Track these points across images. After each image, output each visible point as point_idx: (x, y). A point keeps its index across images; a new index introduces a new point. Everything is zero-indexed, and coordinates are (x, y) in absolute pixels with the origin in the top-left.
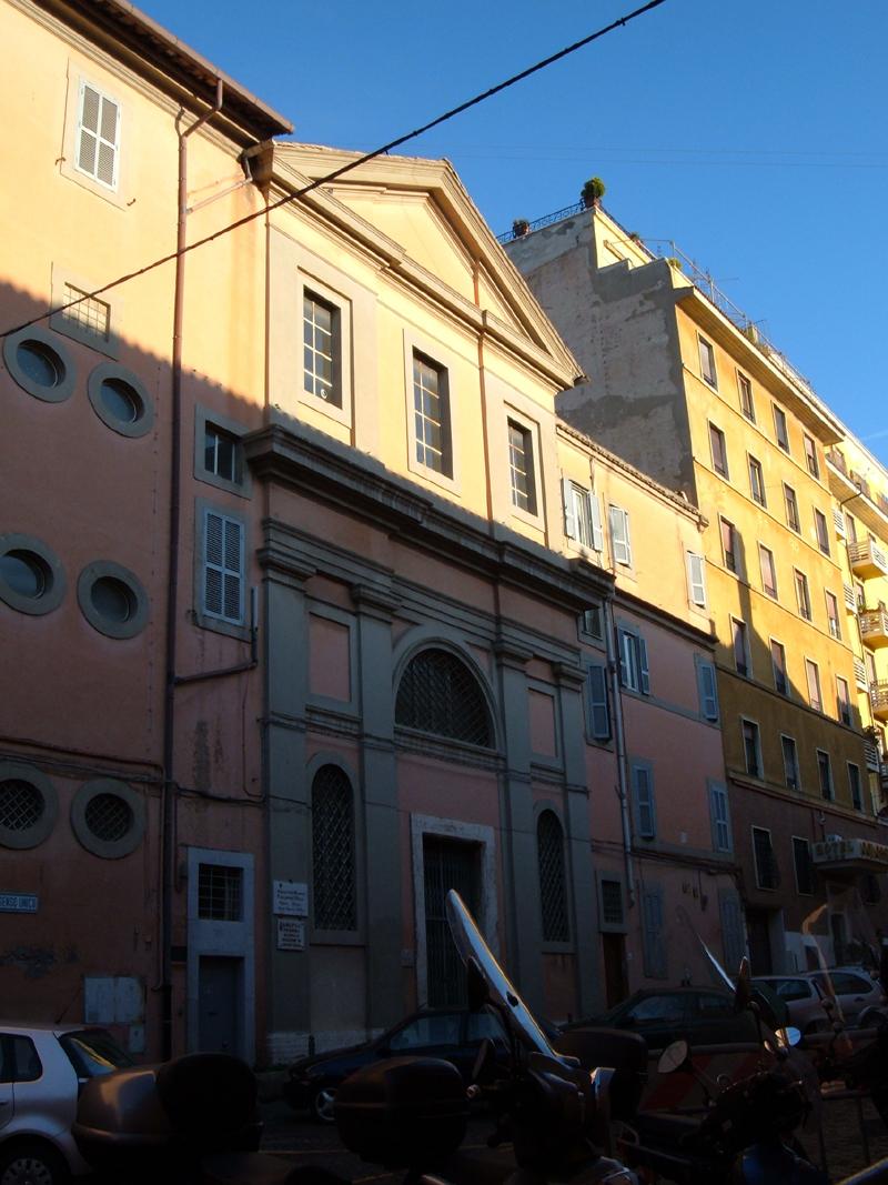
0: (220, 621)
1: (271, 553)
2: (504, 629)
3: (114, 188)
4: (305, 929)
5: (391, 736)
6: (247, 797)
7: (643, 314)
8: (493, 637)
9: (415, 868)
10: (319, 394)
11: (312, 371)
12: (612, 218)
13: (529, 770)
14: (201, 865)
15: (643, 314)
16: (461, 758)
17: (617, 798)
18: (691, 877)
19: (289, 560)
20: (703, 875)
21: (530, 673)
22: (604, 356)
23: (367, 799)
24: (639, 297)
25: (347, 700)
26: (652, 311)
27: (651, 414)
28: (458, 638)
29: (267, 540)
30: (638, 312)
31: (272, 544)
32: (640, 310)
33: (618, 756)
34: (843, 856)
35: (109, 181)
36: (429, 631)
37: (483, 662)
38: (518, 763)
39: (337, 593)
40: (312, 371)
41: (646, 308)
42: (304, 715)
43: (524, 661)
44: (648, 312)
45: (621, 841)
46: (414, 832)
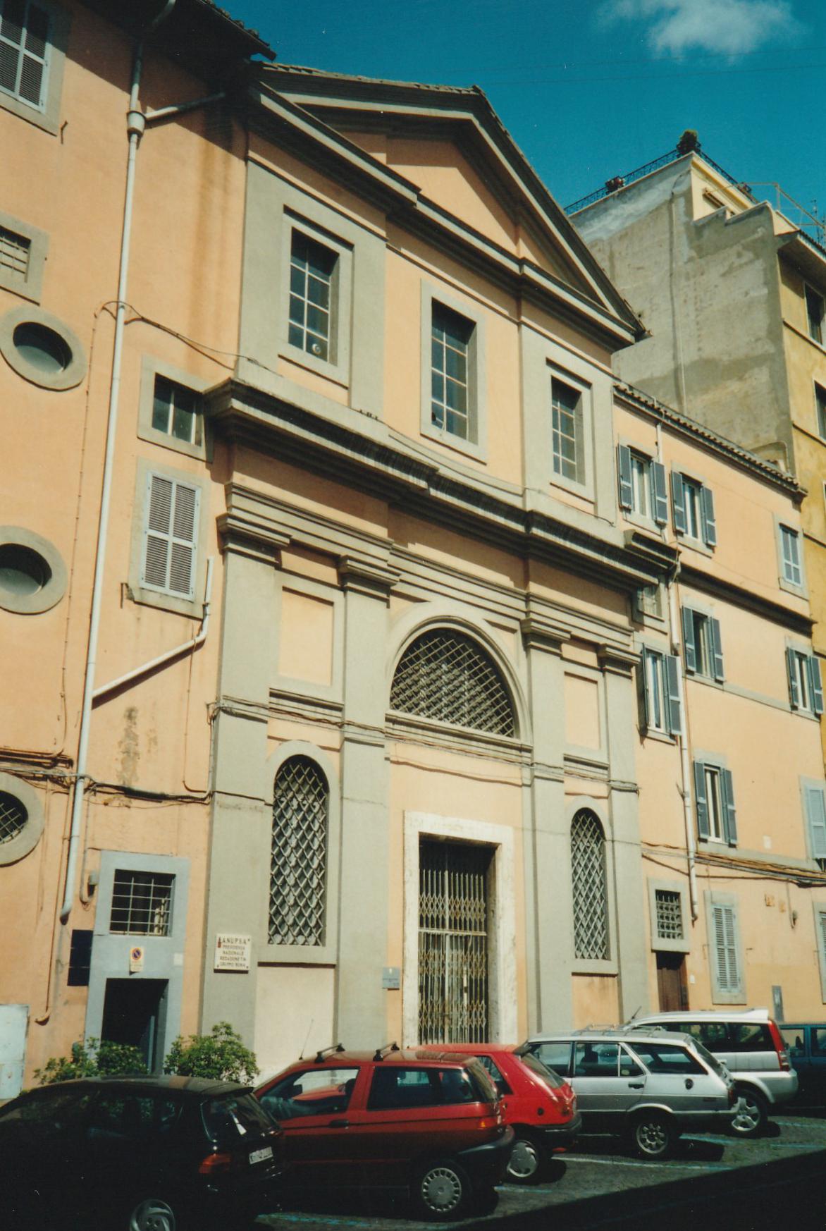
0: (162, 595)
1: (533, 624)
2: (534, 606)
3: (43, 109)
4: (253, 946)
5: (382, 724)
6: (186, 793)
7: (741, 266)
8: (522, 617)
9: (407, 873)
10: (309, 350)
11: (301, 322)
12: (714, 165)
13: (561, 763)
14: (121, 875)
15: (741, 266)
16: (474, 749)
17: (681, 798)
18: (777, 889)
19: (617, 652)
20: (793, 887)
21: (565, 655)
22: (697, 316)
23: (345, 796)
24: (738, 248)
25: (329, 684)
26: (751, 262)
27: (747, 376)
28: (477, 618)
29: (229, 507)
30: (736, 264)
31: (533, 616)
32: (737, 262)
33: (681, 749)
34: (684, 849)
35: (35, 99)
36: (438, 607)
37: (508, 645)
38: (547, 752)
39: (590, 658)
40: (301, 322)
41: (744, 260)
42: (265, 699)
43: (556, 642)
44: (746, 264)
45: (682, 845)
46: (408, 832)
